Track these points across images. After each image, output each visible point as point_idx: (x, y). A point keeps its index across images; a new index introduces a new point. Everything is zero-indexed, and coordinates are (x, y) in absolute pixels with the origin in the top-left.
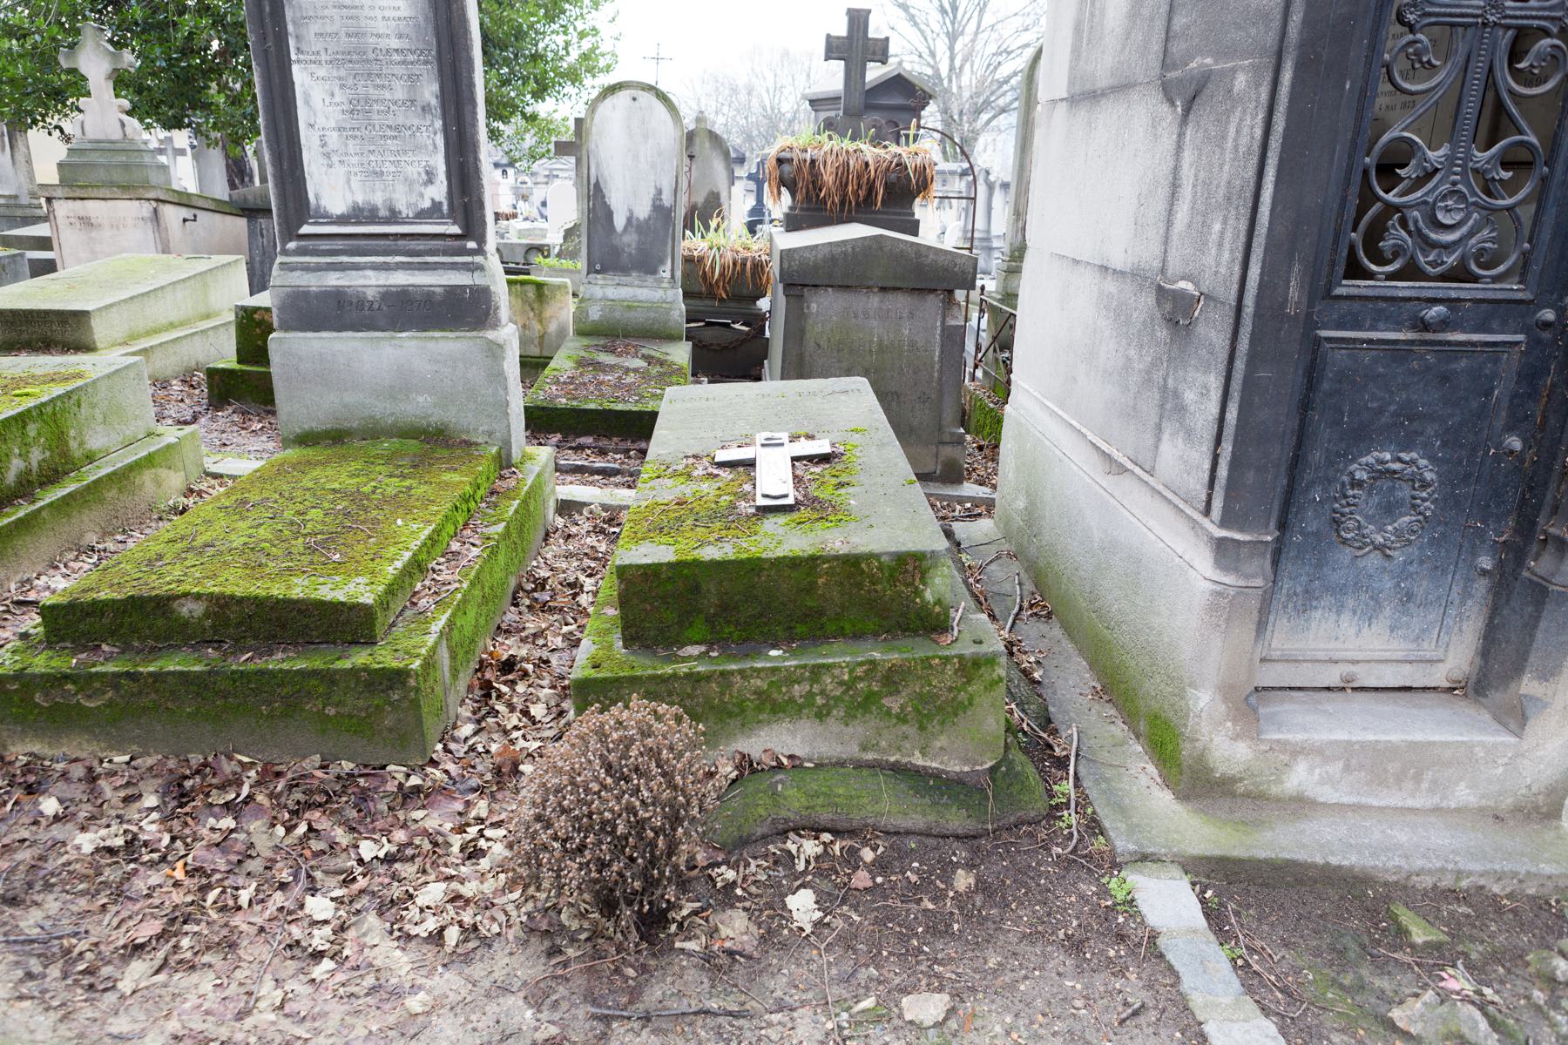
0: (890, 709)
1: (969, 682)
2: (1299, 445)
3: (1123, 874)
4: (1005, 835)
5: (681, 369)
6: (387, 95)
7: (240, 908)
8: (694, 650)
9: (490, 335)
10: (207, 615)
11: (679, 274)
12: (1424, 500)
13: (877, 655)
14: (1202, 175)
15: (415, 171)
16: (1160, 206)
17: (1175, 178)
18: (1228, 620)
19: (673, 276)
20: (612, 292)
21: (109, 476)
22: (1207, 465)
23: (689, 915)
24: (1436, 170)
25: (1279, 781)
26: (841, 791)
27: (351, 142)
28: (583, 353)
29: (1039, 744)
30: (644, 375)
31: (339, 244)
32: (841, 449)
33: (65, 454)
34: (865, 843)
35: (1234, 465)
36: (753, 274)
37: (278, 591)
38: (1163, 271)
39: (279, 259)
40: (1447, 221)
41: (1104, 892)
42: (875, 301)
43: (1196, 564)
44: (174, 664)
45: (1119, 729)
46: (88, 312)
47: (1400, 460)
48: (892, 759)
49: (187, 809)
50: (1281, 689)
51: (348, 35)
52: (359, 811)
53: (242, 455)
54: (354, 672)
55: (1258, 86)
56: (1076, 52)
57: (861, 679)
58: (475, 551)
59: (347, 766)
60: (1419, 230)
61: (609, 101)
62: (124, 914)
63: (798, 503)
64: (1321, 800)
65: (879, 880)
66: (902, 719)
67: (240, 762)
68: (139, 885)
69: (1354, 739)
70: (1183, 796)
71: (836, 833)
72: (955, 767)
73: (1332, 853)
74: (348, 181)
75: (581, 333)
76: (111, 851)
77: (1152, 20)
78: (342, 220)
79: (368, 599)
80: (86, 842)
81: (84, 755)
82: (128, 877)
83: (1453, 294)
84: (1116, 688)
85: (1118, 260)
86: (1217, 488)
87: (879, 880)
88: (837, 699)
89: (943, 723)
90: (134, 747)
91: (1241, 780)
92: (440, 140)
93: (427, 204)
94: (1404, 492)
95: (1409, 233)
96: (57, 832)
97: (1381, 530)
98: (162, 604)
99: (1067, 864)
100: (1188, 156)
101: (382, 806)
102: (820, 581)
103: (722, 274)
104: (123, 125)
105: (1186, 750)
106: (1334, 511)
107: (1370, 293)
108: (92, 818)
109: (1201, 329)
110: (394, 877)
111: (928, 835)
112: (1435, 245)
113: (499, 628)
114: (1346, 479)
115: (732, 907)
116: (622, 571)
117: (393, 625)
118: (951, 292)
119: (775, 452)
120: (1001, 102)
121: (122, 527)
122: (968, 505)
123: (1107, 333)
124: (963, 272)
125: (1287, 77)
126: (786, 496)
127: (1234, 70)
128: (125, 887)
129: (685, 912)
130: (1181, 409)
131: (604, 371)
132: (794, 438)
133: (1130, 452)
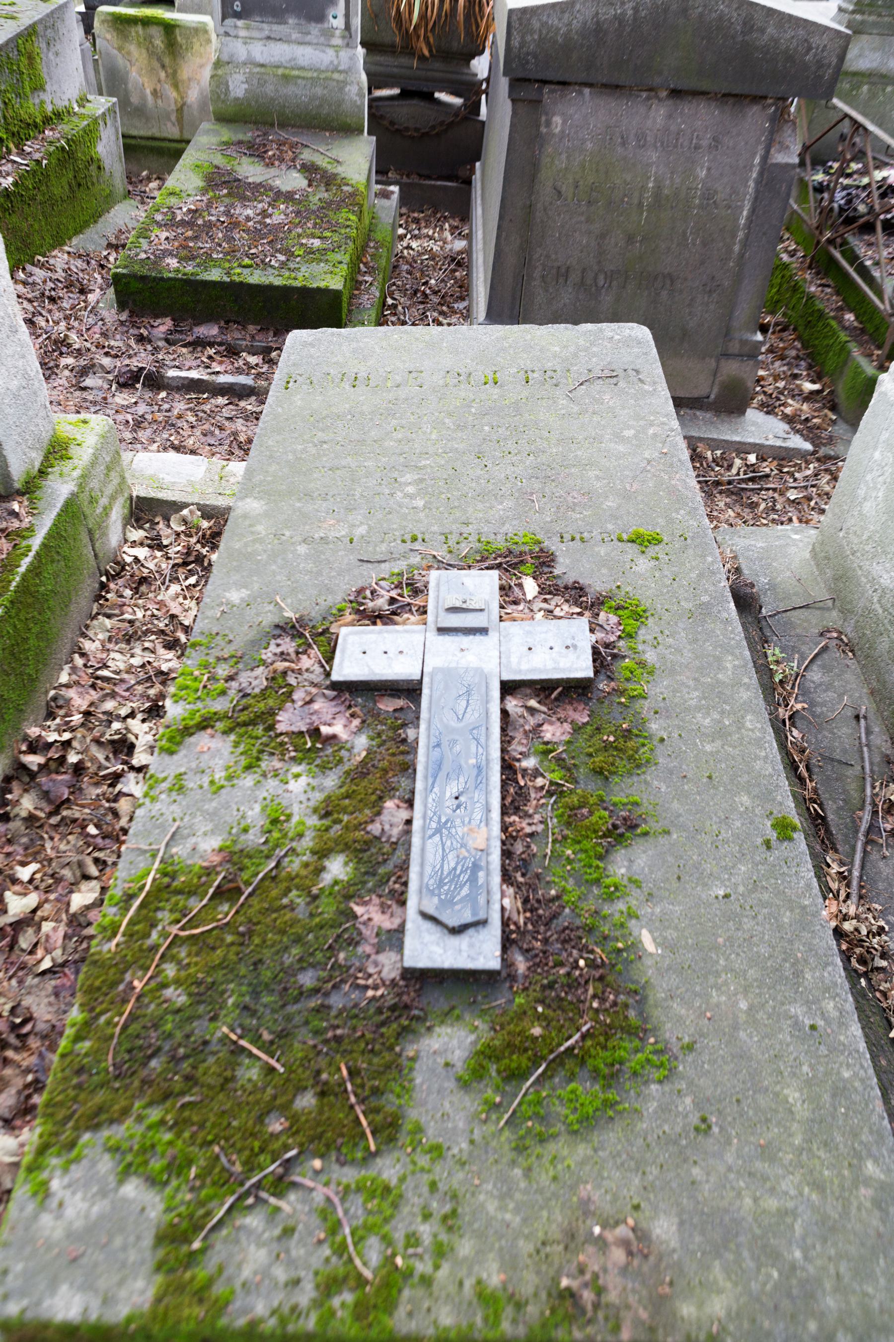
11: (357, 22)
20: (261, 52)
28: (219, 160)
36: (467, 17)
42: (658, 115)
75: (223, 119)
103: (423, 16)
122: (752, 458)
124: (820, 64)
131: (243, 198)
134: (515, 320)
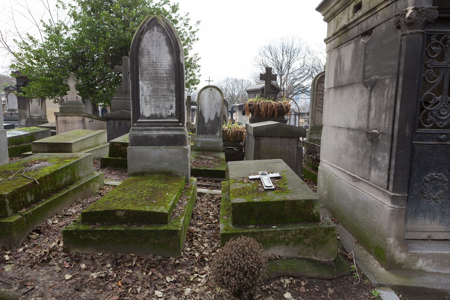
0: (306, 242)
1: (327, 235)
2: (410, 171)
3: (375, 289)
4: (340, 279)
5: (224, 159)
6: (162, 88)
7: (137, 293)
8: (252, 226)
9: (185, 147)
10: (124, 215)
11: (221, 134)
12: (445, 186)
13: (302, 227)
14: (378, 104)
15: (167, 106)
16: (366, 112)
17: (369, 105)
18: (397, 218)
19: (220, 135)
20: (203, 139)
21: (85, 183)
22: (386, 176)
23: (258, 298)
24: (439, 102)
25: (414, 265)
26: (294, 265)
27: (152, 99)
29: (344, 257)
30: (214, 161)
31: (147, 124)
32: (282, 176)
33: (74, 177)
34: (302, 280)
35: (395, 176)
36: (240, 135)
37: (142, 209)
38: (368, 128)
39: (132, 128)
40: (443, 114)
41: (371, 295)
42: (279, 140)
43: (386, 203)
44: (116, 228)
45: (365, 252)
46: (71, 143)
47: (437, 175)
48: (307, 257)
49: (119, 267)
50: (410, 239)
51: (154, 74)
52: (164, 269)
53: (113, 181)
54: (164, 231)
55: (392, 82)
56: (336, 76)
57: (298, 234)
58: (186, 202)
59: (160, 257)
60: (436, 117)
61: (204, 91)
62: (107, 294)
63: (275, 188)
64: (427, 271)
65: (307, 290)
66: (309, 245)
67: (131, 255)
68: (110, 287)
69: (435, 252)
70: (388, 269)
71: (294, 278)
72: (324, 260)
73: (434, 285)
74: (151, 108)
76: (101, 278)
77: (359, 68)
78: (148, 118)
79: (166, 211)
80: (94, 275)
81: (90, 253)
82: (107, 285)
83: (447, 132)
84: (362, 240)
85: (353, 126)
86: (390, 182)
87: (307, 290)
88: (292, 240)
89: (320, 247)
90: (103, 251)
91: (404, 264)
92: (174, 98)
93: (170, 114)
94: (440, 184)
95: (434, 117)
96: (86, 273)
97: (434, 194)
98: (113, 212)
99: (359, 287)
100: (373, 100)
101: (170, 268)
102: (286, 207)
103: (232, 135)
104: (77, 97)
105: (387, 255)
106: (421, 189)
107: (425, 132)
108: (95, 269)
109: (381, 142)
110: (177, 286)
111: (319, 279)
112: (441, 120)
113: (190, 224)
114: (423, 180)
115: (269, 296)
116: (233, 204)
117: (170, 219)
118: (299, 138)
119: (266, 175)
120: (295, 92)
121: (85, 197)
123: (351, 145)
125: (401, 80)
126: (272, 186)
127: (385, 79)
128: (106, 287)
129: (257, 297)
130: (377, 163)
132: (269, 173)
133: (361, 175)
134: (259, 158)
